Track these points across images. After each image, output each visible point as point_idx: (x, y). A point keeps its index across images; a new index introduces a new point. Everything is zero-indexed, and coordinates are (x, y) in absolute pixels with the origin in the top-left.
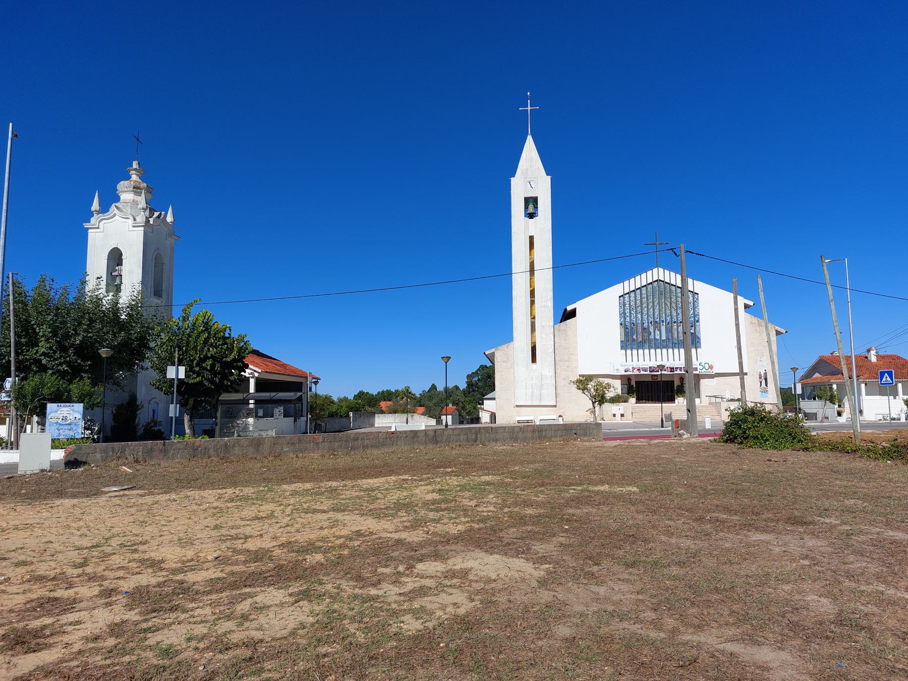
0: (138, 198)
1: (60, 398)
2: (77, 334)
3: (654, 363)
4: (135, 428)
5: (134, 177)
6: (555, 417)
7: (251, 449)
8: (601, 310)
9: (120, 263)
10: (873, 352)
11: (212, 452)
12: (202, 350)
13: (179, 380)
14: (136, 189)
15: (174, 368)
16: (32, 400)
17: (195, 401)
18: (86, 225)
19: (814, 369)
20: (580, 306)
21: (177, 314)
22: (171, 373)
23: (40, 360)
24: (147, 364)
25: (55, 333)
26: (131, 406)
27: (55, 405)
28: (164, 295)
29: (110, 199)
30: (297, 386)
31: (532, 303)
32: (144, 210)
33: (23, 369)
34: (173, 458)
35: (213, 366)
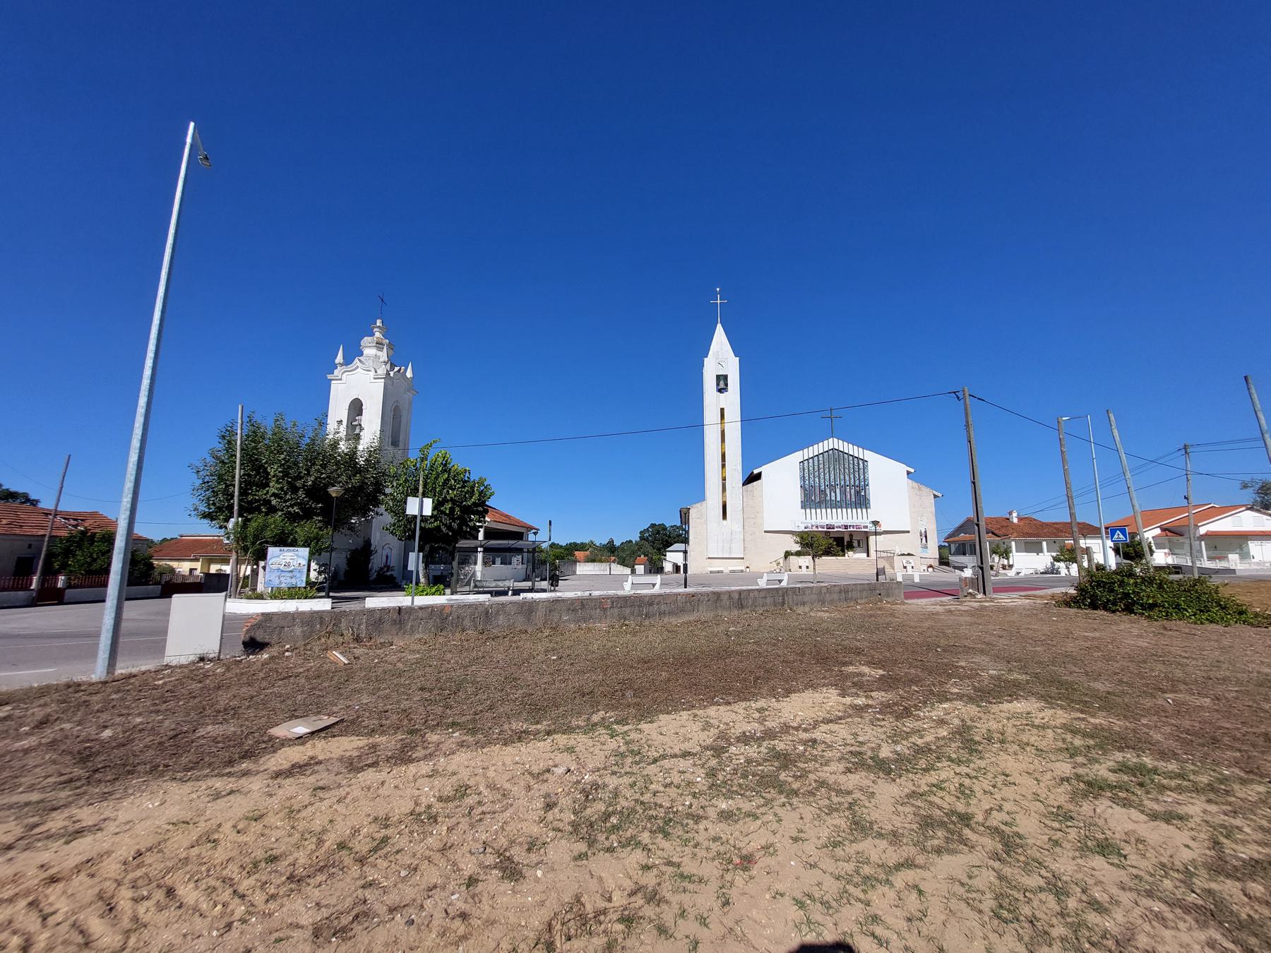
0: (379, 353)
1: (284, 540)
2: (308, 474)
3: (845, 521)
4: (368, 571)
5: (378, 334)
6: (743, 568)
7: (521, 619)
8: (783, 476)
9: (360, 414)
10: (1015, 515)
11: (467, 623)
12: (441, 493)
13: (424, 519)
14: (379, 345)
15: (417, 500)
16: (253, 543)
17: (432, 547)
18: (329, 377)
19: (961, 529)
20: (765, 470)
21: (414, 455)
22: (412, 506)
23: (270, 501)
24: (382, 509)
25: (286, 474)
26: (363, 553)
27: (277, 549)
28: (401, 446)
29: (353, 353)
30: (519, 536)
31: (723, 466)
32: (386, 363)
33: (247, 509)
34: (412, 632)
35: (452, 510)
